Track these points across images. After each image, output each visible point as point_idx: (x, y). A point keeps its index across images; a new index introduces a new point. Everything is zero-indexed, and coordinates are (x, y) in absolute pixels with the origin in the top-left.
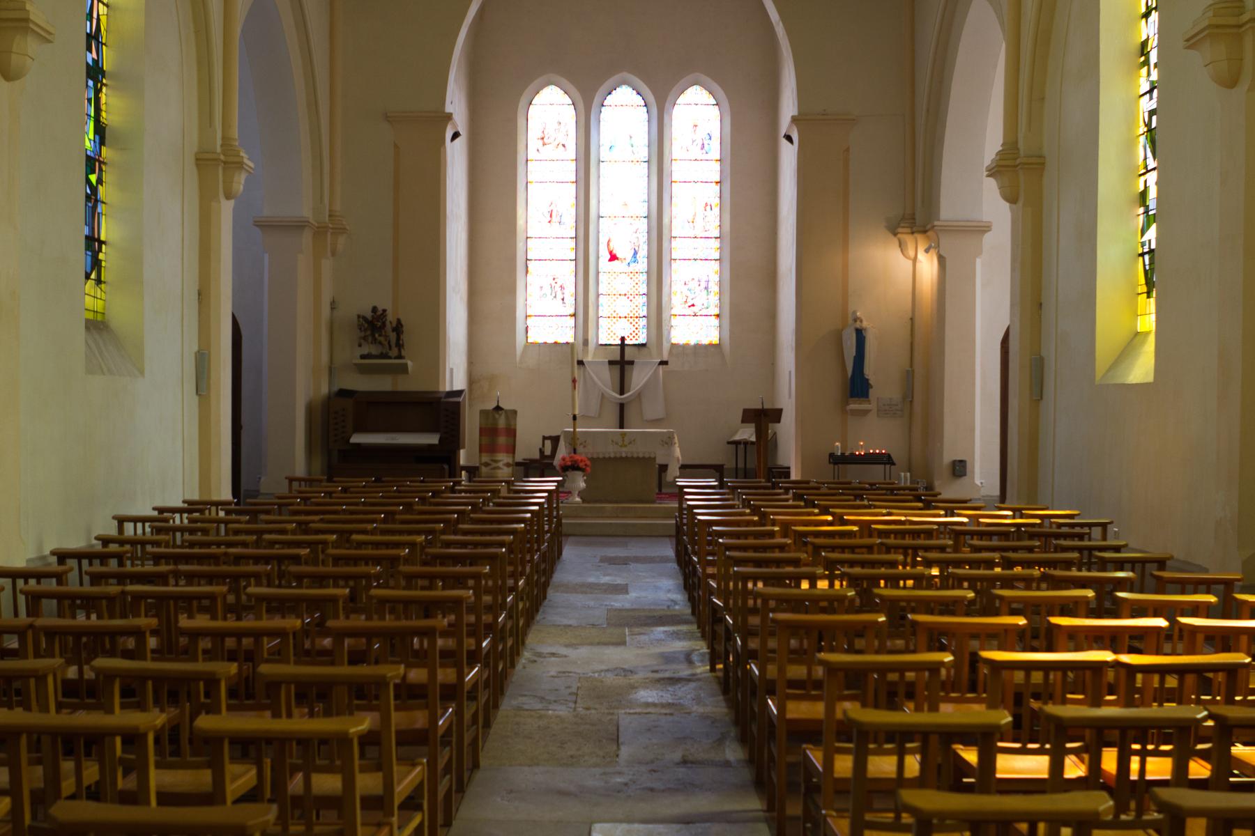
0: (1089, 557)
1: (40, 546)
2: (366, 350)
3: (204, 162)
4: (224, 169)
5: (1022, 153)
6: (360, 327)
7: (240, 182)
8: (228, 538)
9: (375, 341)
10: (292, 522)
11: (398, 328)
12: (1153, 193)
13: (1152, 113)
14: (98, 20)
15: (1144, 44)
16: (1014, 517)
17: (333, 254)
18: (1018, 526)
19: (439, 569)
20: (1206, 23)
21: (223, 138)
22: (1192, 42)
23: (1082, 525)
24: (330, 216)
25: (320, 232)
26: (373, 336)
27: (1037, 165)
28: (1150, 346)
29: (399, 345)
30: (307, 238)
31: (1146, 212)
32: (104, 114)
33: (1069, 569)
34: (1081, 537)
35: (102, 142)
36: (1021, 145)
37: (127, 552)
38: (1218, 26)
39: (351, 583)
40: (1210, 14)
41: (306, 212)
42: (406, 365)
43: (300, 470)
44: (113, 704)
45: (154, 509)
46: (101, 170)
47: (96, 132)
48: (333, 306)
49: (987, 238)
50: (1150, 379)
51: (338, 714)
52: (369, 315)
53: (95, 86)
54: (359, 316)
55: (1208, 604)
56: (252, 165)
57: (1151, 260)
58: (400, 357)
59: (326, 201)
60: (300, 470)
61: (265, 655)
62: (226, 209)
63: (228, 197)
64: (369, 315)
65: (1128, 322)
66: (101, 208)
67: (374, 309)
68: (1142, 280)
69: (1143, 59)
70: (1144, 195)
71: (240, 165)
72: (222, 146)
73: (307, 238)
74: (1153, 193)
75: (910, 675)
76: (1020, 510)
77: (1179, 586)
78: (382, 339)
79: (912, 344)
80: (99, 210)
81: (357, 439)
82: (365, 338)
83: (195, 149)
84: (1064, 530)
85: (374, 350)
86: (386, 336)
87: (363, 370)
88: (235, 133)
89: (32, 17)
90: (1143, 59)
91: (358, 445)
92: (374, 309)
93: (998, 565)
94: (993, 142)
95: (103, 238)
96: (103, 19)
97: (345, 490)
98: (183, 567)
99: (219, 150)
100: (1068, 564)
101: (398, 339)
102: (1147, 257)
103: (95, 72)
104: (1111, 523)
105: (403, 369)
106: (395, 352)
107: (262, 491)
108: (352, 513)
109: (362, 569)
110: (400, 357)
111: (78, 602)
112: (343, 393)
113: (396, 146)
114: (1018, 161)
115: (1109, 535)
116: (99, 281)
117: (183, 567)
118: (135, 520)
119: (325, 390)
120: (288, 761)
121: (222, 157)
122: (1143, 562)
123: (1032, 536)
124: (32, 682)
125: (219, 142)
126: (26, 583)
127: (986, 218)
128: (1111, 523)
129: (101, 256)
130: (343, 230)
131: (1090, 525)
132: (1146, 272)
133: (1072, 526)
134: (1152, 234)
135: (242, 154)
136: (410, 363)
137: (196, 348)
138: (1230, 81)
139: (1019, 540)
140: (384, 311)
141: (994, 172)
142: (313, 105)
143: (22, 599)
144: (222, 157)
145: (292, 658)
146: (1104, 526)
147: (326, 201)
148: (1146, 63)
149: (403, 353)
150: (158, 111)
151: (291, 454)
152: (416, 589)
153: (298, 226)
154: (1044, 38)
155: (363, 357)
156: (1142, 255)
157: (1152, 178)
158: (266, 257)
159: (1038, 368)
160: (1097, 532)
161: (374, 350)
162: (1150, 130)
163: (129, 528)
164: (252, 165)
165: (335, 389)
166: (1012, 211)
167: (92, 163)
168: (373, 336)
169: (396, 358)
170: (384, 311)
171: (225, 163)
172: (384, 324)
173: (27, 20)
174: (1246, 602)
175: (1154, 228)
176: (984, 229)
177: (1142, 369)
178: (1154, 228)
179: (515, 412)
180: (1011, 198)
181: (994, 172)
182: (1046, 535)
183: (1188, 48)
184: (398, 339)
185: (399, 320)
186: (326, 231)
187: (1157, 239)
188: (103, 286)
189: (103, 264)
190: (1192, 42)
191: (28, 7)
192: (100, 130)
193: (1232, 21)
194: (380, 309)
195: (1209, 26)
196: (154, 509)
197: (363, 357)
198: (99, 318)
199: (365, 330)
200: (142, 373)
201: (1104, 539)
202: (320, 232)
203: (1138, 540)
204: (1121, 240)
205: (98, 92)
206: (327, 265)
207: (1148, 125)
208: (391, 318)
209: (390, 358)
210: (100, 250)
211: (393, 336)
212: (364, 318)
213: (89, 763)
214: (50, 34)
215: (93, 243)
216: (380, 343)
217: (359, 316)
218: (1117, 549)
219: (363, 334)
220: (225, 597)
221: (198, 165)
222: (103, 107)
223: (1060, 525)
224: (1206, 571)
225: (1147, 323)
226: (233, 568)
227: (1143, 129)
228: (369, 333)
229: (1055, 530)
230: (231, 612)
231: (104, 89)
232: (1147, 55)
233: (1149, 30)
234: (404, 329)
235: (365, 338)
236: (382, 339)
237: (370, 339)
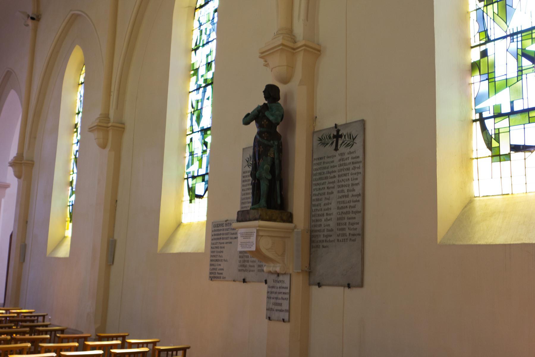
0: (33, 330)
5: (25, 159)
12: (74, 183)
13: (77, 151)
15: (76, 125)
16: (6, 313)
18: (6, 317)
20: (96, 124)
22: (91, 130)
23: (34, 316)
27: (31, 164)
28: (68, 243)
31: (72, 189)
33: (24, 335)
34: (33, 321)
36: (25, 155)
38: (100, 126)
40: (98, 121)
49: (8, 191)
50: (68, 256)
55: (75, 346)
57: (72, 208)
65: (61, 233)
68: (69, 216)
69: (75, 130)
70: (71, 183)
74: (74, 183)
76: (9, 310)
77: (67, 340)
79: (111, 246)
84: (29, 318)
90: (75, 130)
93: (27, 333)
94: (13, 152)
100: (24, 333)
102: (71, 207)
104: (47, 315)
114: (23, 162)
115: (45, 320)
122: (56, 331)
123: (11, 321)
127: (8, 181)
128: (47, 315)
131: (38, 316)
132: (70, 213)
133: (31, 316)
134: (73, 198)
138: (103, 146)
139: (6, 323)
141: (12, 164)
146: (44, 316)
148: (77, 131)
154: (38, 114)
156: (69, 206)
157: (75, 176)
159: (24, 248)
160: (41, 319)
162: (76, 158)
166: (19, 182)
174: (43, 347)
175: (74, 196)
176: (6, 186)
177: (64, 251)
178: (74, 196)
179: (211, 279)
180: (19, 177)
181: (12, 164)
182: (16, 321)
183: (90, 131)
187: (75, 201)
190: (91, 130)
193: (105, 125)
195: (97, 125)
201: (44, 321)
203: (56, 322)
204: (62, 201)
207: (76, 155)
218: (46, 326)
223: (25, 317)
224: (82, 333)
225: (69, 233)
227: (73, 157)
229: (23, 319)
232: (77, 129)
233: (78, 119)
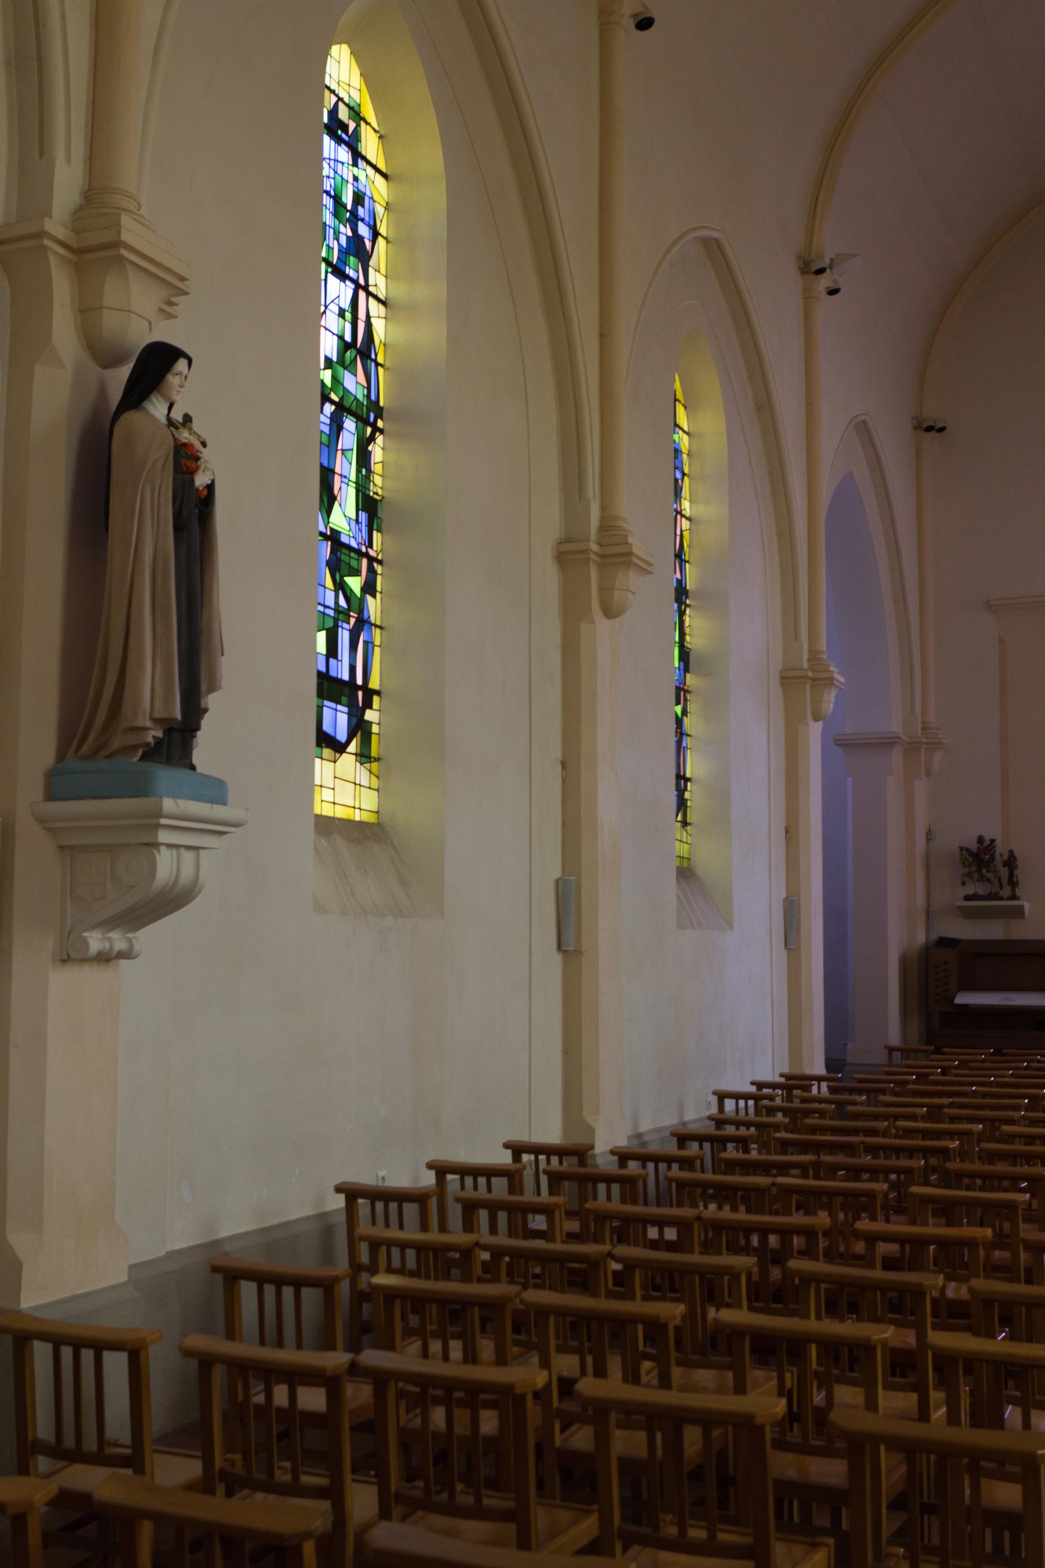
1: (636, 1124)
2: (970, 890)
3: (790, 680)
4: (812, 686)
6: (963, 862)
7: (829, 700)
8: (759, 1119)
9: (982, 878)
10: (922, 1106)
11: (1011, 862)
14: (682, 536)
17: (928, 774)
19: (1026, 1169)
21: (810, 651)
24: (923, 729)
25: (912, 748)
26: (980, 872)
29: (1013, 883)
30: (897, 756)
32: (688, 638)
33: (952, 1103)
35: (686, 670)
37: (751, 1136)
39: (893, 1177)
41: (896, 727)
42: (1022, 907)
43: (895, 1038)
44: (809, 1311)
45: (752, 1083)
46: (685, 699)
47: (680, 659)
48: (929, 836)
51: (1037, 1342)
52: (974, 846)
53: (679, 608)
54: (961, 849)
56: (842, 680)
58: (1014, 897)
59: (918, 710)
60: (895, 1038)
61: (479, 1272)
62: (815, 731)
63: (816, 719)
64: (974, 846)
66: (687, 742)
67: (980, 840)
71: (830, 681)
72: (809, 660)
73: (897, 756)
75: (697, 1533)
78: (990, 875)
80: (684, 745)
81: (963, 999)
82: (969, 875)
83: (780, 667)
85: (981, 889)
86: (996, 872)
87: (968, 914)
88: (823, 644)
89: (635, 551)
91: (966, 1006)
92: (980, 840)
95: (688, 775)
96: (686, 534)
97: (963, 1064)
98: (826, 1158)
99: (806, 665)
101: (1011, 875)
103: (681, 593)
105: (1019, 912)
106: (1007, 891)
107: (850, 1059)
108: (984, 1095)
109: (904, 1162)
110: (1014, 897)
111: (711, 1191)
112: (944, 943)
113: (1001, 640)
116: (685, 823)
117: (826, 1158)
118: (736, 1096)
119: (921, 938)
120: (1005, 1392)
121: (810, 674)
124: (726, 1278)
125: (806, 656)
126: (669, 1168)
129: (687, 795)
130: (939, 745)
135: (832, 668)
136: (1027, 905)
137: (784, 895)
140: (993, 841)
142: (900, 599)
143: (544, 1179)
144: (810, 674)
145: (982, 1274)
147: (918, 710)
149: (1018, 893)
150: (741, 631)
151: (889, 1022)
152: (960, 1189)
153: (886, 743)
155: (968, 898)
158: (850, 780)
161: (981, 889)
163: (729, 1105)
164: (842, 680)
165: (934, 937)
167: (681, 693)
168: (980, 872)
169: (1009, 899)
170: (993, 841)
171: (813, 680)
172: (993, 856)
173: (630, 554)
184: (1011, 875)
185: (1011, 852)
186: (919, 746)
188: (689, 828)
189: (375, 729)
191: (630, 540)
192: (685, 655)
194: (987, 838)
196: (752, 1083)
197: (968, 898)
198: (685, 865)
199: (970, 866)
200: (731, 925)
202: (912, 748)
205: (682, 614)
206: (921, 786)
208: (1000, 849)
209: (1001, 899)
210: (686, 789)
211: (1004, 872)
212: (968, 850)
213: (760, 1374)
214: (650, 564)
215: (682, 780)
216: (988, 880)
217: (961, 849)
219: (966, 870)
220: (886, 1195)
221: (782, 684)
222: (687, 631)
226: (987, 1168)
228: (974, 868)
230: (865, 1211)
231: (688, 611)
234: (1018, 862)
235: (969, 875)
236: (990, 875)
237: (976, 875)
